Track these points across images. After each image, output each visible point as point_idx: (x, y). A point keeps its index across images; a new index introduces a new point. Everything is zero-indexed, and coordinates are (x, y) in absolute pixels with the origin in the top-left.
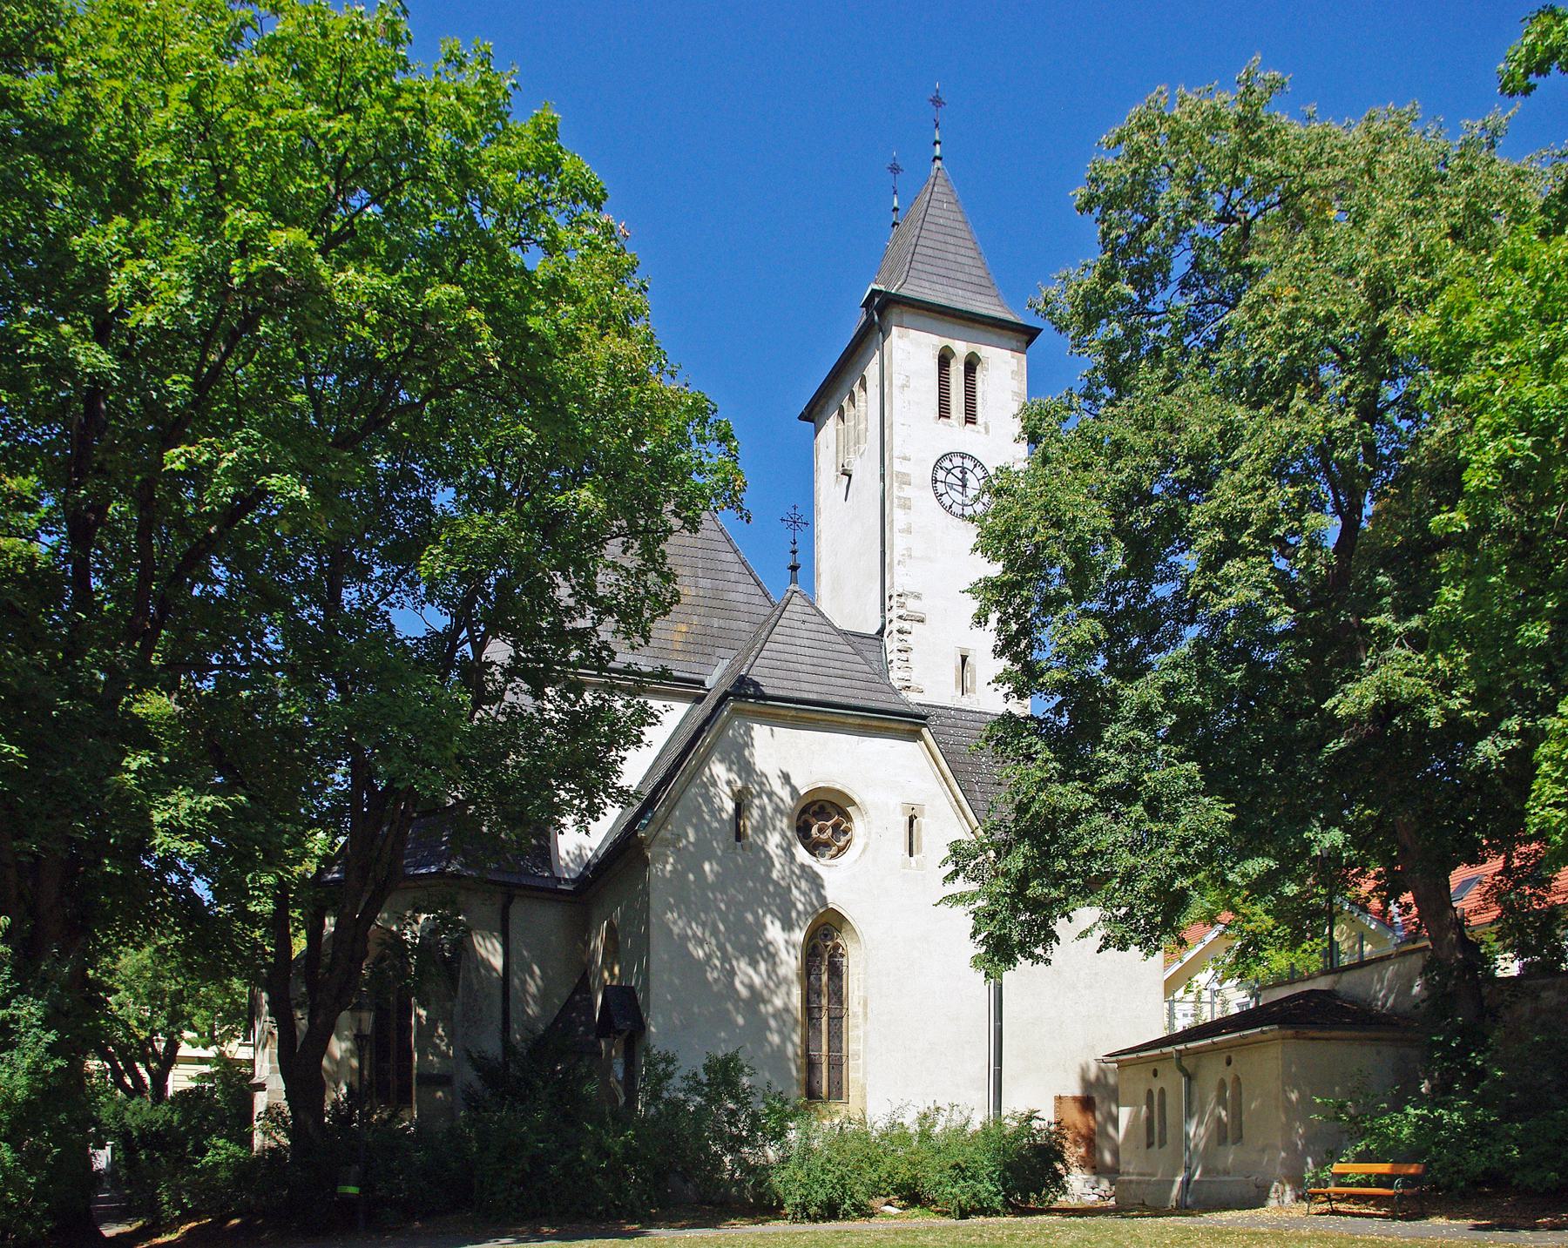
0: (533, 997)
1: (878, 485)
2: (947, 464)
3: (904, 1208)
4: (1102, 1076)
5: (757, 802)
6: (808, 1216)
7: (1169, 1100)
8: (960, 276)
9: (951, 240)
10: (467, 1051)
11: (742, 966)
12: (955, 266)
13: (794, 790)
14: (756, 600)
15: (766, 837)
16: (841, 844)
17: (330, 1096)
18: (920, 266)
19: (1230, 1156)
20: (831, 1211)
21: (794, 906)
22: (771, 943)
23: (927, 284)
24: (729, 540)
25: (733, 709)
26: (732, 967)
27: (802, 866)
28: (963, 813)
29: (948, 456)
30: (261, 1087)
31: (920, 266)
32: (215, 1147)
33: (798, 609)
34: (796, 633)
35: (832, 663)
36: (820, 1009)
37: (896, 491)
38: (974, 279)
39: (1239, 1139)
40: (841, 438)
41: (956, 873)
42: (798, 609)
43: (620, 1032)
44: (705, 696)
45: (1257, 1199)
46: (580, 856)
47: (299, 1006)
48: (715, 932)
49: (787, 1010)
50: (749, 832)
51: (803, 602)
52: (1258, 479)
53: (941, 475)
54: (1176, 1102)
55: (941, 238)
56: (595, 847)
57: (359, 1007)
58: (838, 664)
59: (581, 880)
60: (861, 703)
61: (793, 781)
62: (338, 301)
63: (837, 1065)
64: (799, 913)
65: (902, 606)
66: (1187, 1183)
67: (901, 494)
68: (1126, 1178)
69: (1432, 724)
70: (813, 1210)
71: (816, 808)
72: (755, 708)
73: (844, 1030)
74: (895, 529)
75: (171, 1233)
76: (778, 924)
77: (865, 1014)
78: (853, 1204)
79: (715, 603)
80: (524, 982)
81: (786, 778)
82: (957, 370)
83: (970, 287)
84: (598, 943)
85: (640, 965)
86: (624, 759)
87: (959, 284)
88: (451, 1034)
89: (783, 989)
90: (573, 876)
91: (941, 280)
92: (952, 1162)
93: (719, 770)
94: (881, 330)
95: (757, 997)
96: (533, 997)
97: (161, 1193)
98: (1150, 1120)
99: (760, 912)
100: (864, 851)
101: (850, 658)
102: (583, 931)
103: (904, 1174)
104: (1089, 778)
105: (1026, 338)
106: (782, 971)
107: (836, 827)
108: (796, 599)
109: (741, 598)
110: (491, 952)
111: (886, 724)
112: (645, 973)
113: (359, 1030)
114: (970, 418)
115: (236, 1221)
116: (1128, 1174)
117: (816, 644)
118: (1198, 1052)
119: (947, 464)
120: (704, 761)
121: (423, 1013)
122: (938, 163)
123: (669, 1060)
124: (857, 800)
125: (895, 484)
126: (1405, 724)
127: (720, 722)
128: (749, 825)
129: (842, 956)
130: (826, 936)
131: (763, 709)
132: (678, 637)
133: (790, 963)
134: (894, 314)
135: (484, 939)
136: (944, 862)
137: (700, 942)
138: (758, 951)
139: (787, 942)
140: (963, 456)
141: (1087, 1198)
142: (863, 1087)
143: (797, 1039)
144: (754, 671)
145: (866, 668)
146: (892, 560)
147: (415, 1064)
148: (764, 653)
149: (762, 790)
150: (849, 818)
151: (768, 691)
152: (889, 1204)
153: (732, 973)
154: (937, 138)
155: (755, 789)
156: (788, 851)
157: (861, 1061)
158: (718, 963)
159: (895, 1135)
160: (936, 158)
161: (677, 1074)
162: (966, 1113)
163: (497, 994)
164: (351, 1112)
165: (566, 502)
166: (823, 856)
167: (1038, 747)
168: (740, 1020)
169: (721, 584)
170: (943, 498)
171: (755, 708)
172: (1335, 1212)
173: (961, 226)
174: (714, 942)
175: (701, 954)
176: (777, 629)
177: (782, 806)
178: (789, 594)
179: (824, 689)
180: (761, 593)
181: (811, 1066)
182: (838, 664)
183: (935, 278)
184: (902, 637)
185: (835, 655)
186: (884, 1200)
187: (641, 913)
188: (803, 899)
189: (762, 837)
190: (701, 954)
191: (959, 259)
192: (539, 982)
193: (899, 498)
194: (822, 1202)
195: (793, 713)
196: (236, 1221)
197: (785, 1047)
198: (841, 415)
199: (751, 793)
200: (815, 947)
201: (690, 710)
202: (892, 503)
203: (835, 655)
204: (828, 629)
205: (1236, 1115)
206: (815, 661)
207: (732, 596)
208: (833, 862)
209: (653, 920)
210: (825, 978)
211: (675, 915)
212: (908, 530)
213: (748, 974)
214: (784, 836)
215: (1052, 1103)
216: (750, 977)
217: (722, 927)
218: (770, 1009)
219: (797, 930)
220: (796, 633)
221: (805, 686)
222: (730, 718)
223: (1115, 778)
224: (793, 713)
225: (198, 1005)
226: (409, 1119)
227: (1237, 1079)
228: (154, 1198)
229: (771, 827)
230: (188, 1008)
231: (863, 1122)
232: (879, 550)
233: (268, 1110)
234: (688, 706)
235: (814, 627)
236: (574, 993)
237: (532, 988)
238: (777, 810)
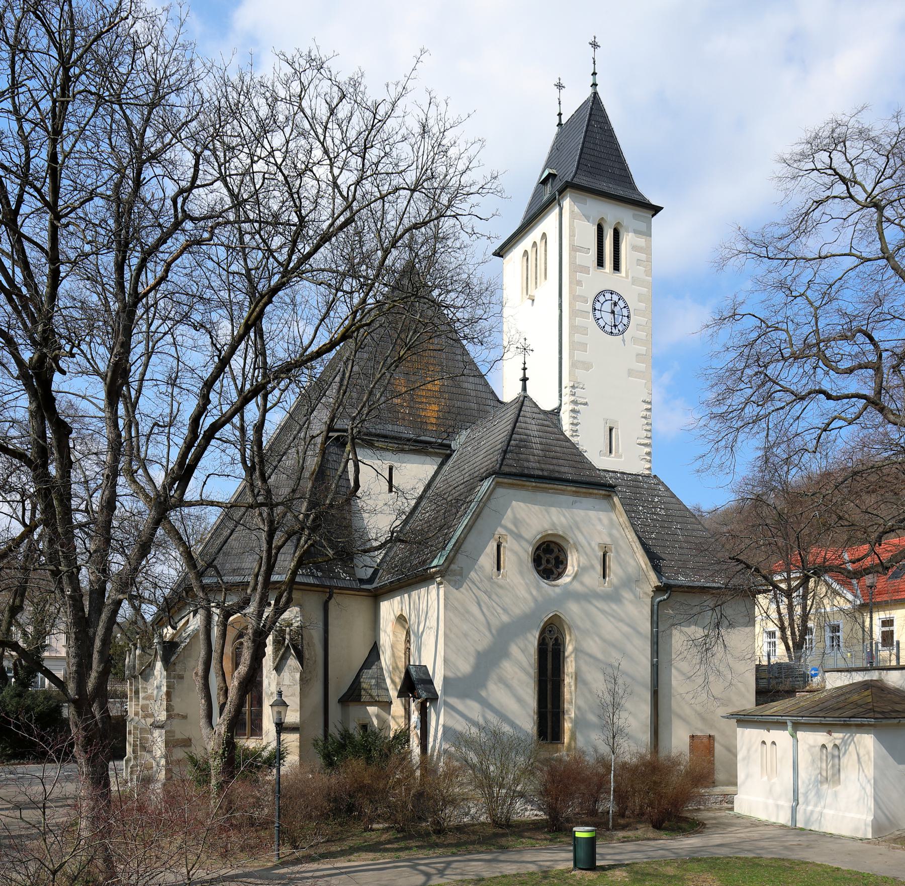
114: (616, 267)
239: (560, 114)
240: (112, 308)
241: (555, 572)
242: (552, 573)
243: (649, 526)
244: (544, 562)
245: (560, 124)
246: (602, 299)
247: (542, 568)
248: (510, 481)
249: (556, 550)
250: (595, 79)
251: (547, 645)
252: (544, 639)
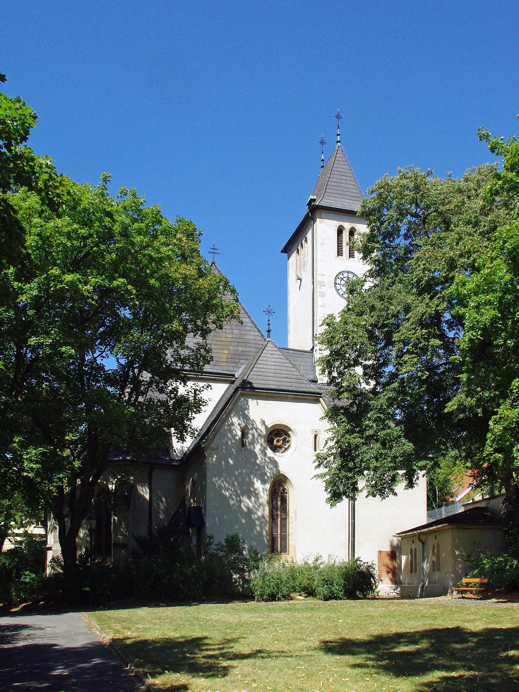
0: (162, 510)
1: (311, 286)
3: (306, 597)
4: (399, 544)
5: (251, 432)
6: (263, 600)
7: (417, 553)
8: (348, 193)
9: (344, 178)
10: (133, 534)
11: (245, 499)
12: (345, 189)
13: (266, 427)
14: (258, 338)
15: (254, 447)
16: (286, 447)
17: (79, 553)
18: (329, 191)
19: (437, 575)
20: (272, 597)
21: (266, 474)
22: (256, 489)
23: (332, 198)
24: (246, 313)
25: (241, 393)
26: (240, 498)
27: (270, 458)
29: (342, 273)
30: (50, 549)
31: (329, 191)
32: (25, 575)
33: (270, 349)
34: (268, 359)
35: (283, 372)
36: (277, 515)
37: (318, 289)
38: (354, 195)
39: (439, 569)
40: (298, 262)
41: (319, 465)
42: (270, 349)
43: (195, 526)
44: (235, 381)
45: (444, 593)
46: (182, 450)
47: (67, 517)
48: (233, 486)
49: (263, 516)
50: (247, 444)
51: (272, 346)
52: (413, 326)
53: (338, 281)
54: (419, 553)
55: (339, 177)
56: (188, 446)
57: (90, 519)
58: (285, 372)
59: (182, 460)
60: (294, 389)
61: (266, 424)
62: (85, 294)
63: (284, 538)
64: (268, 477)
66: (423, 587)
67: (321, 291)
68: (404, 585)
69: (479, 415)
70: (265, 597)
71: (276, 432)
72: (249, 393)
73: (287, 524)
74: (318, 305)
75: (16, 608)
76: (259, 481)
77: (296, 517)
78: (282, 595)
79: (240, 340)
80: (158, 505)
81: (263, 422)
82: (346, 235)
83: (352, 198)
84: (189, 487)
85: (203, 498)
86: (194, 418)
87: (347, 197)
88: (127, 527)
89: (262, 508)
90: (179, 459)
92: (323, 578)
93: (235, 420)
94: (312, 219)
95: (250, 512)
96: (162, 510)
97: (13, 592)
98: (411, 561)
99: (252, 477)
100: (295, 450)
101: (291, 369)
102: (183, 482)
103: (305, 583)
104: (361, 432)
106: (261, 500)
107: (284, 440)
108: (269, 345)
109: (251, 337)
110: (145, 492)
111: (304, 397)
112: (205, 501)
113: (91, 527)
115: (42, 603)
116: (405, 584)
117: (277, 364)
118: (426, 533)
119: (341, 276)
120: (228, 415)
121: (116, 518)
122: (339, 144)
123: (211, 537)
124: (292, 429)
125: (318, 286)
126: (470, 415)
127: (235, 399)
128: (247, 441)
129: (287, 493)
130: (280, 485)
131: (255, 393)
132: (224, 356)
133: (264, 497)
134: (318, 213)
135: (142, 487)
136: (314, 462)
137: (227, 489)
138: (251, 493)
139: (263, 489)
140: (348, 272)
141: (391, 594)
142: (295, 548)
143: (267, 528)
144: (249, 377)
145: (298, 373)
147: (113, 539)
148: (254, 369)
149: (253, 427)
150: (289, 436)
151: (255, 386)
152: (300, 595)
153: (240, 501)
154: (339, 133)
155: (250, 426)
156: (264, 452)
157: (294, 537)
158: (234, 497)
159: (307, 567)
160: (338, 142)
161: (214, 543)
162: (334, 558)
163: (147, 510)
164: (87, 558)
165: (168, 327)
166: (278, 452)
167: (344, 420)
168: (243, 521)
169: (242, 332)
170: (339, 291)
171: (249, 393)
172: (463, 598)
173: (349, 171)
174: (233, 489)
175: (227, 494)
176: (260, 358)
177: (261, 433)
178: (266, 342)
179: (279, 383)
180: (260, 335)
181: (273, 540)
182: (285, 372)
184: (321, 352)
185: (284, 368)
186: (298, 594)
187: (203, 476)
188: (270, 471)
189: (252, 446)
190: (227, 494)
191: (347, 186)
192: (165, 504)
193: (320, 292)
194: (269, 594)
195: (266, 394)
196: (42, 603)
197: (262, 532)
198: (298, 252)
199: (248, 428)
200: (275, 489)
201: (229, 387)
202: (317, 294)
203: (284, 368)
205: (438, 559)
206: (276, 371)
207: (247, 337)
208: (283, 454)
209: (208, 480)
210: (279, 503)
211: (217, 479)
212: (324, 306)
213: (247, 502)
214: (262, 445)
215: (376, 554)
216: (248, 504)
217: (236, 483)
218: (256, 516)
219: (267, 484)
220: (268, 359)
221: (270, 382)
222: (239, 398)
223: (370, 432)
224: (266, 394)
225: (17, 510)
226: (109, 563)
227: (438, 545)
228: (9, 593)
229: (256, 442)
230: (13, 512)
231: (292, 562)
233: (53, 559)
234: (228, 385)
235: (276, 356)
236: (178, 509)
237: (162, 507)
238: (259, 435)
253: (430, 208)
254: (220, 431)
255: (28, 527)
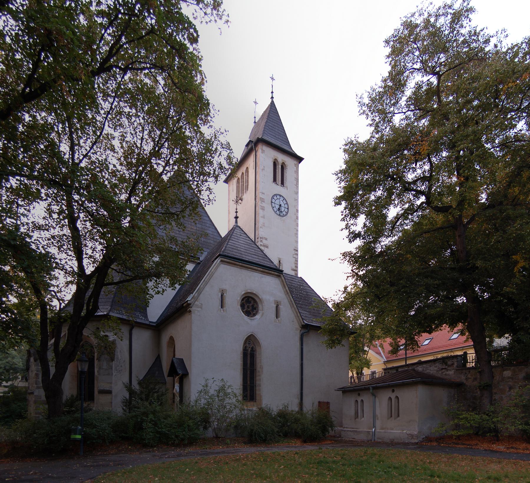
2: (275, 198)
28: (293, 305)
35: (251, 250)
37: (259, 203)
65: (261, 241)
87: (279, 140)
91: (274, 137)
105: (299, 161)
109: (211, 232)
114: (282, 183)
146: (258, 226)
183: (272, 136)
201: (221, 237)
204: (248, 239)
206: (246, 249)
220: (239, 238)
221: (244, 256)
232: (254, 223)
239: (255, 117)
240: (152, 415)
241: (252, 313)
242: (250, 314)
243: (298, 298)
244: (246, 307)
245: (255, 122)
246: (275, 198)
247: (245, 310)
248: (228, 260)
249: (252, 302)
250: (272, 95)
251: (247, 350)
252: (246, 347)
253: (455, 21)
254: (205, 289)
255: (14, 381)
